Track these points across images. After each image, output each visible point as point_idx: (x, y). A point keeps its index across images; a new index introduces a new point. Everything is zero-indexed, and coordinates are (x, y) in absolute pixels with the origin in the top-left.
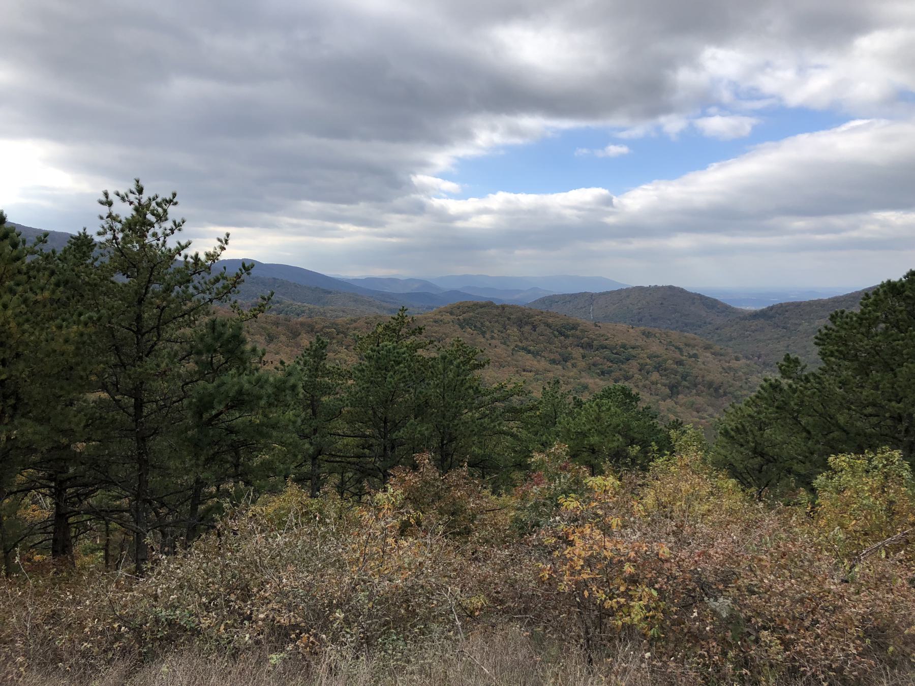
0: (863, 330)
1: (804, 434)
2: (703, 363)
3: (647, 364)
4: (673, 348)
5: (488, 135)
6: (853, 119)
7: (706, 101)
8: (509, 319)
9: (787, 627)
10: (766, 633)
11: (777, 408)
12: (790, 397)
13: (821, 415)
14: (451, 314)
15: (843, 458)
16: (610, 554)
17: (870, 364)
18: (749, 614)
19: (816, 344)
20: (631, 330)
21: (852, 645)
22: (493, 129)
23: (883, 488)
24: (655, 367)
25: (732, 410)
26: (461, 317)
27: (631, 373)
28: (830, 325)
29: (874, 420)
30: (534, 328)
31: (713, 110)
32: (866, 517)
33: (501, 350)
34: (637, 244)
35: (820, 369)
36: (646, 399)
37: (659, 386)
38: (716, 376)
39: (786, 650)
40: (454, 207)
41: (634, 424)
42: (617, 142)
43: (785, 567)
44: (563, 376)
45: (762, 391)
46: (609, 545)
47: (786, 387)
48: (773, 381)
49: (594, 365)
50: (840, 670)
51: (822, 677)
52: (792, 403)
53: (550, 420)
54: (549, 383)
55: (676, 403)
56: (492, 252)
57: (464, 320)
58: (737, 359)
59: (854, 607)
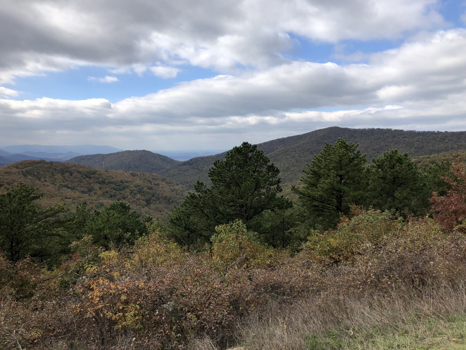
0: (228, 168)
1: (206, 217)
2: (162, 188)
3: (134, 190)
4: (147, 181)
5: (34, 65)
6: (219, 74)
7: (154, 58)
8: (55, 169)
9: (198, 309)
10: (189, 314)
11: (194, 206)
14: (17, 168)
16: (114, 291)
17: (231, 183)
20: (125, 173)
21: (225, 310)
22: (37, 61)
24: (138, 191)
25: (175, 209)
26: (24, 170)
27: (126, 195)
28: (214, 167)
29: (233, 208)
30: (71, 174)
31: (158, 63)
32: (232, 251)
33: (51, 188)
34: (125, 129)
36: (134, 208)
37: (141, 201)
38: (168, 194)
39: (198, 319)
40: (14, 104)
41: (128, 221)
42: (110, 75)
43: (197, 281)
44: (89, 200)
46: (113, 286)
49: (106, 192)
50: (221, 323)
51: (213, 328)
53: (81, 224)
54: (80, 204)
55: (150, 209)
56: (42, 132)
57: (26, 171)
58: (177, 185)
59: (225, 293)
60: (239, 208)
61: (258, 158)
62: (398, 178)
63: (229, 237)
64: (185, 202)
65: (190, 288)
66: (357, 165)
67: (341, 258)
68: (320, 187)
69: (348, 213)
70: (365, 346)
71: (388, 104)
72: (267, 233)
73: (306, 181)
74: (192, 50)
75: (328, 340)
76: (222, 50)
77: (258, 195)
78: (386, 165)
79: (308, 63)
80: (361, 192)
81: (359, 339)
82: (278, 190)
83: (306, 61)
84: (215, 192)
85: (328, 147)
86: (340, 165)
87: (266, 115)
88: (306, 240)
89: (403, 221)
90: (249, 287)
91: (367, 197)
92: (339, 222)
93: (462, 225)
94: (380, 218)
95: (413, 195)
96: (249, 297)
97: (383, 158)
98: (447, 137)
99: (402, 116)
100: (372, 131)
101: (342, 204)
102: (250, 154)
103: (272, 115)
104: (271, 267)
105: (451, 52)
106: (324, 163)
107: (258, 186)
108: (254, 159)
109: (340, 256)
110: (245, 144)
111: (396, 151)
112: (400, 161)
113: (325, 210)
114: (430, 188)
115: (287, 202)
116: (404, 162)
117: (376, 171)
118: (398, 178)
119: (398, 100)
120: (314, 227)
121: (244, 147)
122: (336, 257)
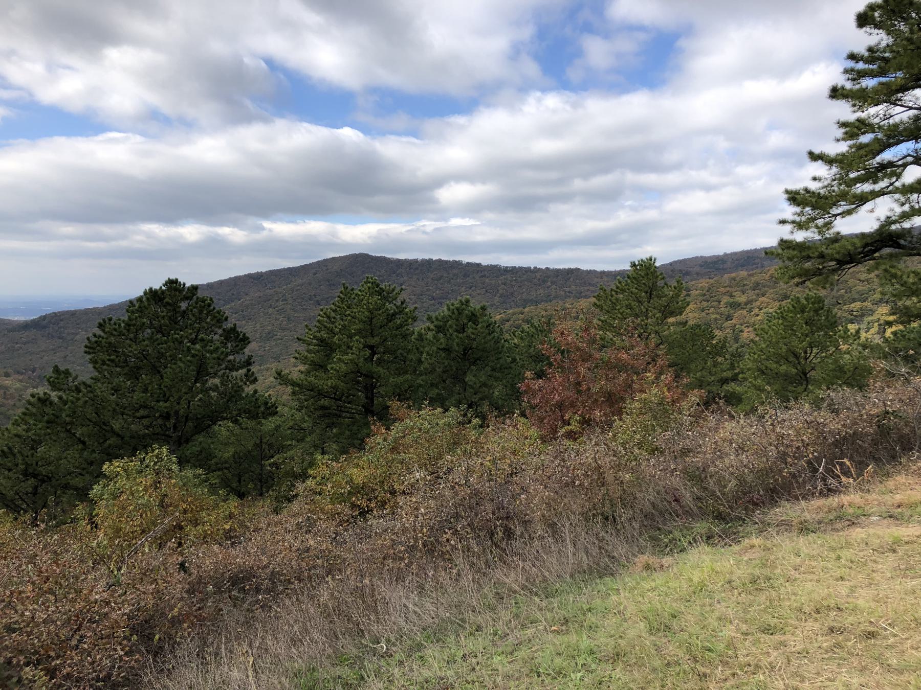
0: (132, 336)
1: (80, 446)
9: (52, 654)
10: (28, 669)
12: (61, 410)
13: (95, 424)
15: (117, 464)
17: (139, 368)
18: (9, 655)
19: (86, 352)
21: (119, 648)
23: (156, 485)
28: (99, 332)
29: (146, 422)
32: (141, 516)
35: (92, 378)
45: (29, 407)
47: (56, 400)
48: (42, 395)
50: (109, 676)
52: (64, 415)
59: (120, 609)
60: (160, 421)
61: (201, 312)
62: (471, 349)
63: (134, 484)
64: (24, 414)
65: (31, 611)
66: (401, 326)
67: (373, 505)
68: (332, 368)
69: (385, 418)
70: (407, 669)
71: (455, 216)
72: (226, 468)
73: (306, 358)
74: (38, 68)
75: (338, 671)
76: (116, 78)
77: (202, 391)
78: (451, 327)
79: (306, 125)
80: (408, 377)
81: (397, 657)
82: (248, 380)
83: (302, 120)
84: (102, 389)
85: (347, 292)
86: (370, 327)
87: (222, 224)
88: (304, 476)
89: (481, 426)
90: (177, 586)
91: (420, 386)
92: (368, 436)
93: (570, 427)
94: (441, 422)
95: (496, 379)
96: (176, 610)
97: (447, 313)
98: (548, 277)
99: (479, 238)
100: (428, 264)
101: (375, 402)
102: (184, 305)
103: (235, 224)
104: (230, 537)
105: (553, 131)
106: (339, 324)
107: (201, 372)
108: (194, 315)
109: (370, 500)
110: (173, 284)
111: (468, 301)
112: (473, 318)
113: (344, 414)
114: (523, 366)
115: (266, 403)
116: (480, 320)
117: (435, 337)
118: (471, 349)
119: (472, 209)
120: (323, 449)
121: (169, 289)
122: (363, 504)
